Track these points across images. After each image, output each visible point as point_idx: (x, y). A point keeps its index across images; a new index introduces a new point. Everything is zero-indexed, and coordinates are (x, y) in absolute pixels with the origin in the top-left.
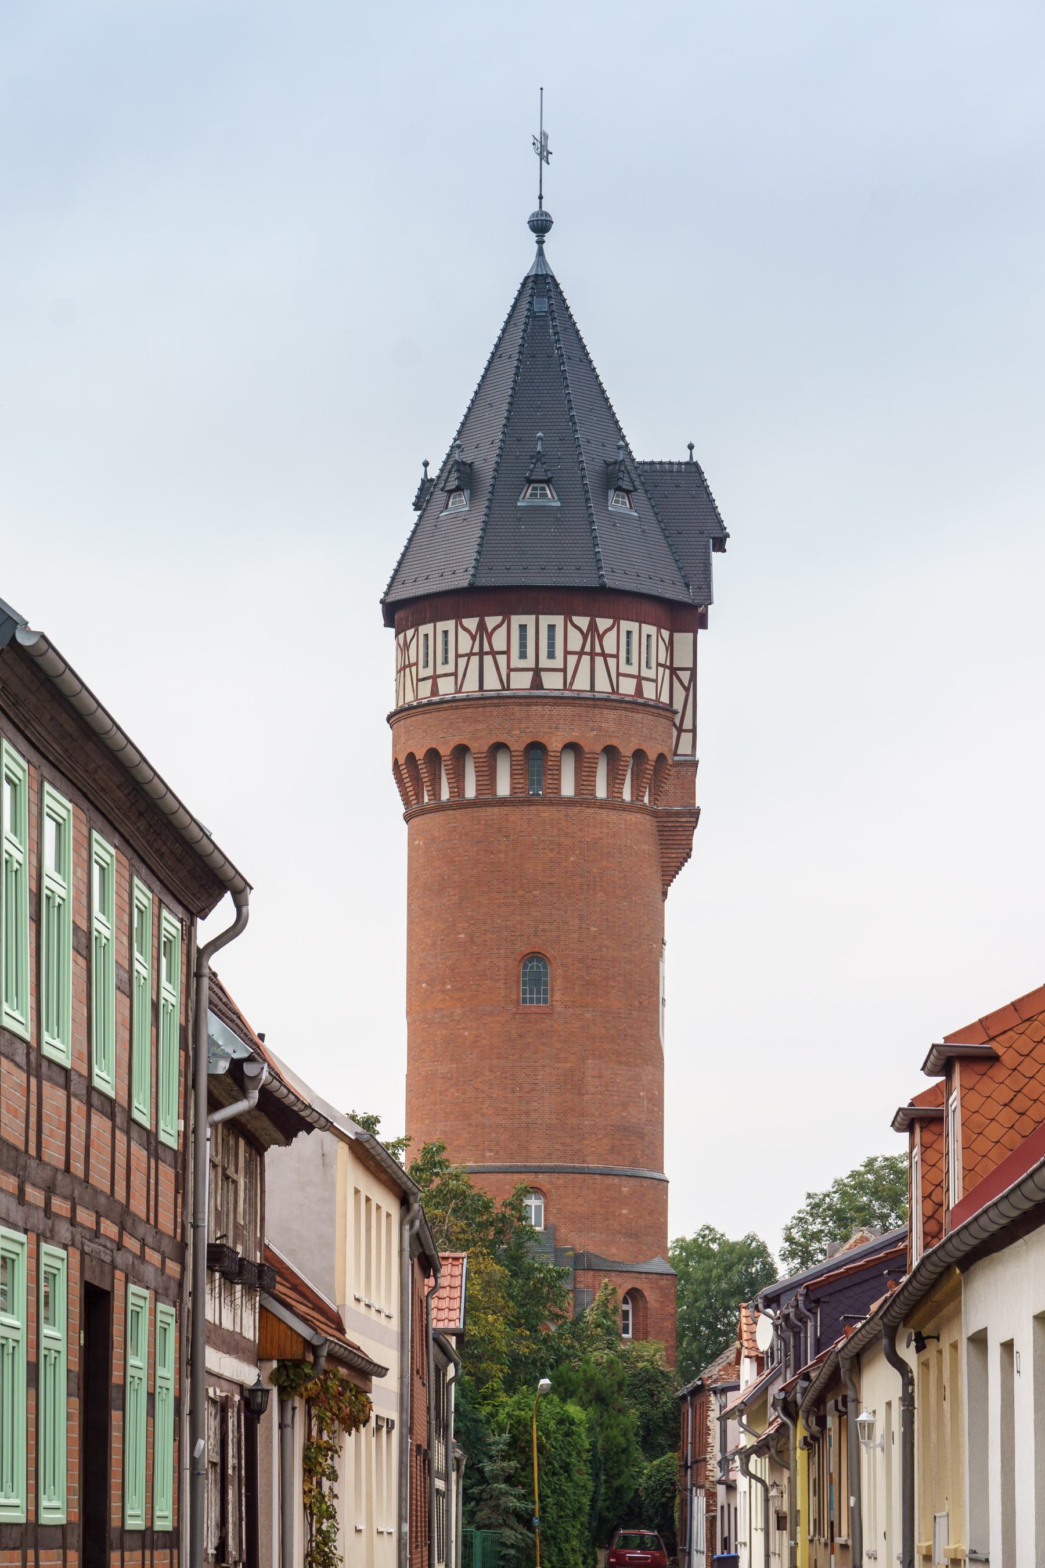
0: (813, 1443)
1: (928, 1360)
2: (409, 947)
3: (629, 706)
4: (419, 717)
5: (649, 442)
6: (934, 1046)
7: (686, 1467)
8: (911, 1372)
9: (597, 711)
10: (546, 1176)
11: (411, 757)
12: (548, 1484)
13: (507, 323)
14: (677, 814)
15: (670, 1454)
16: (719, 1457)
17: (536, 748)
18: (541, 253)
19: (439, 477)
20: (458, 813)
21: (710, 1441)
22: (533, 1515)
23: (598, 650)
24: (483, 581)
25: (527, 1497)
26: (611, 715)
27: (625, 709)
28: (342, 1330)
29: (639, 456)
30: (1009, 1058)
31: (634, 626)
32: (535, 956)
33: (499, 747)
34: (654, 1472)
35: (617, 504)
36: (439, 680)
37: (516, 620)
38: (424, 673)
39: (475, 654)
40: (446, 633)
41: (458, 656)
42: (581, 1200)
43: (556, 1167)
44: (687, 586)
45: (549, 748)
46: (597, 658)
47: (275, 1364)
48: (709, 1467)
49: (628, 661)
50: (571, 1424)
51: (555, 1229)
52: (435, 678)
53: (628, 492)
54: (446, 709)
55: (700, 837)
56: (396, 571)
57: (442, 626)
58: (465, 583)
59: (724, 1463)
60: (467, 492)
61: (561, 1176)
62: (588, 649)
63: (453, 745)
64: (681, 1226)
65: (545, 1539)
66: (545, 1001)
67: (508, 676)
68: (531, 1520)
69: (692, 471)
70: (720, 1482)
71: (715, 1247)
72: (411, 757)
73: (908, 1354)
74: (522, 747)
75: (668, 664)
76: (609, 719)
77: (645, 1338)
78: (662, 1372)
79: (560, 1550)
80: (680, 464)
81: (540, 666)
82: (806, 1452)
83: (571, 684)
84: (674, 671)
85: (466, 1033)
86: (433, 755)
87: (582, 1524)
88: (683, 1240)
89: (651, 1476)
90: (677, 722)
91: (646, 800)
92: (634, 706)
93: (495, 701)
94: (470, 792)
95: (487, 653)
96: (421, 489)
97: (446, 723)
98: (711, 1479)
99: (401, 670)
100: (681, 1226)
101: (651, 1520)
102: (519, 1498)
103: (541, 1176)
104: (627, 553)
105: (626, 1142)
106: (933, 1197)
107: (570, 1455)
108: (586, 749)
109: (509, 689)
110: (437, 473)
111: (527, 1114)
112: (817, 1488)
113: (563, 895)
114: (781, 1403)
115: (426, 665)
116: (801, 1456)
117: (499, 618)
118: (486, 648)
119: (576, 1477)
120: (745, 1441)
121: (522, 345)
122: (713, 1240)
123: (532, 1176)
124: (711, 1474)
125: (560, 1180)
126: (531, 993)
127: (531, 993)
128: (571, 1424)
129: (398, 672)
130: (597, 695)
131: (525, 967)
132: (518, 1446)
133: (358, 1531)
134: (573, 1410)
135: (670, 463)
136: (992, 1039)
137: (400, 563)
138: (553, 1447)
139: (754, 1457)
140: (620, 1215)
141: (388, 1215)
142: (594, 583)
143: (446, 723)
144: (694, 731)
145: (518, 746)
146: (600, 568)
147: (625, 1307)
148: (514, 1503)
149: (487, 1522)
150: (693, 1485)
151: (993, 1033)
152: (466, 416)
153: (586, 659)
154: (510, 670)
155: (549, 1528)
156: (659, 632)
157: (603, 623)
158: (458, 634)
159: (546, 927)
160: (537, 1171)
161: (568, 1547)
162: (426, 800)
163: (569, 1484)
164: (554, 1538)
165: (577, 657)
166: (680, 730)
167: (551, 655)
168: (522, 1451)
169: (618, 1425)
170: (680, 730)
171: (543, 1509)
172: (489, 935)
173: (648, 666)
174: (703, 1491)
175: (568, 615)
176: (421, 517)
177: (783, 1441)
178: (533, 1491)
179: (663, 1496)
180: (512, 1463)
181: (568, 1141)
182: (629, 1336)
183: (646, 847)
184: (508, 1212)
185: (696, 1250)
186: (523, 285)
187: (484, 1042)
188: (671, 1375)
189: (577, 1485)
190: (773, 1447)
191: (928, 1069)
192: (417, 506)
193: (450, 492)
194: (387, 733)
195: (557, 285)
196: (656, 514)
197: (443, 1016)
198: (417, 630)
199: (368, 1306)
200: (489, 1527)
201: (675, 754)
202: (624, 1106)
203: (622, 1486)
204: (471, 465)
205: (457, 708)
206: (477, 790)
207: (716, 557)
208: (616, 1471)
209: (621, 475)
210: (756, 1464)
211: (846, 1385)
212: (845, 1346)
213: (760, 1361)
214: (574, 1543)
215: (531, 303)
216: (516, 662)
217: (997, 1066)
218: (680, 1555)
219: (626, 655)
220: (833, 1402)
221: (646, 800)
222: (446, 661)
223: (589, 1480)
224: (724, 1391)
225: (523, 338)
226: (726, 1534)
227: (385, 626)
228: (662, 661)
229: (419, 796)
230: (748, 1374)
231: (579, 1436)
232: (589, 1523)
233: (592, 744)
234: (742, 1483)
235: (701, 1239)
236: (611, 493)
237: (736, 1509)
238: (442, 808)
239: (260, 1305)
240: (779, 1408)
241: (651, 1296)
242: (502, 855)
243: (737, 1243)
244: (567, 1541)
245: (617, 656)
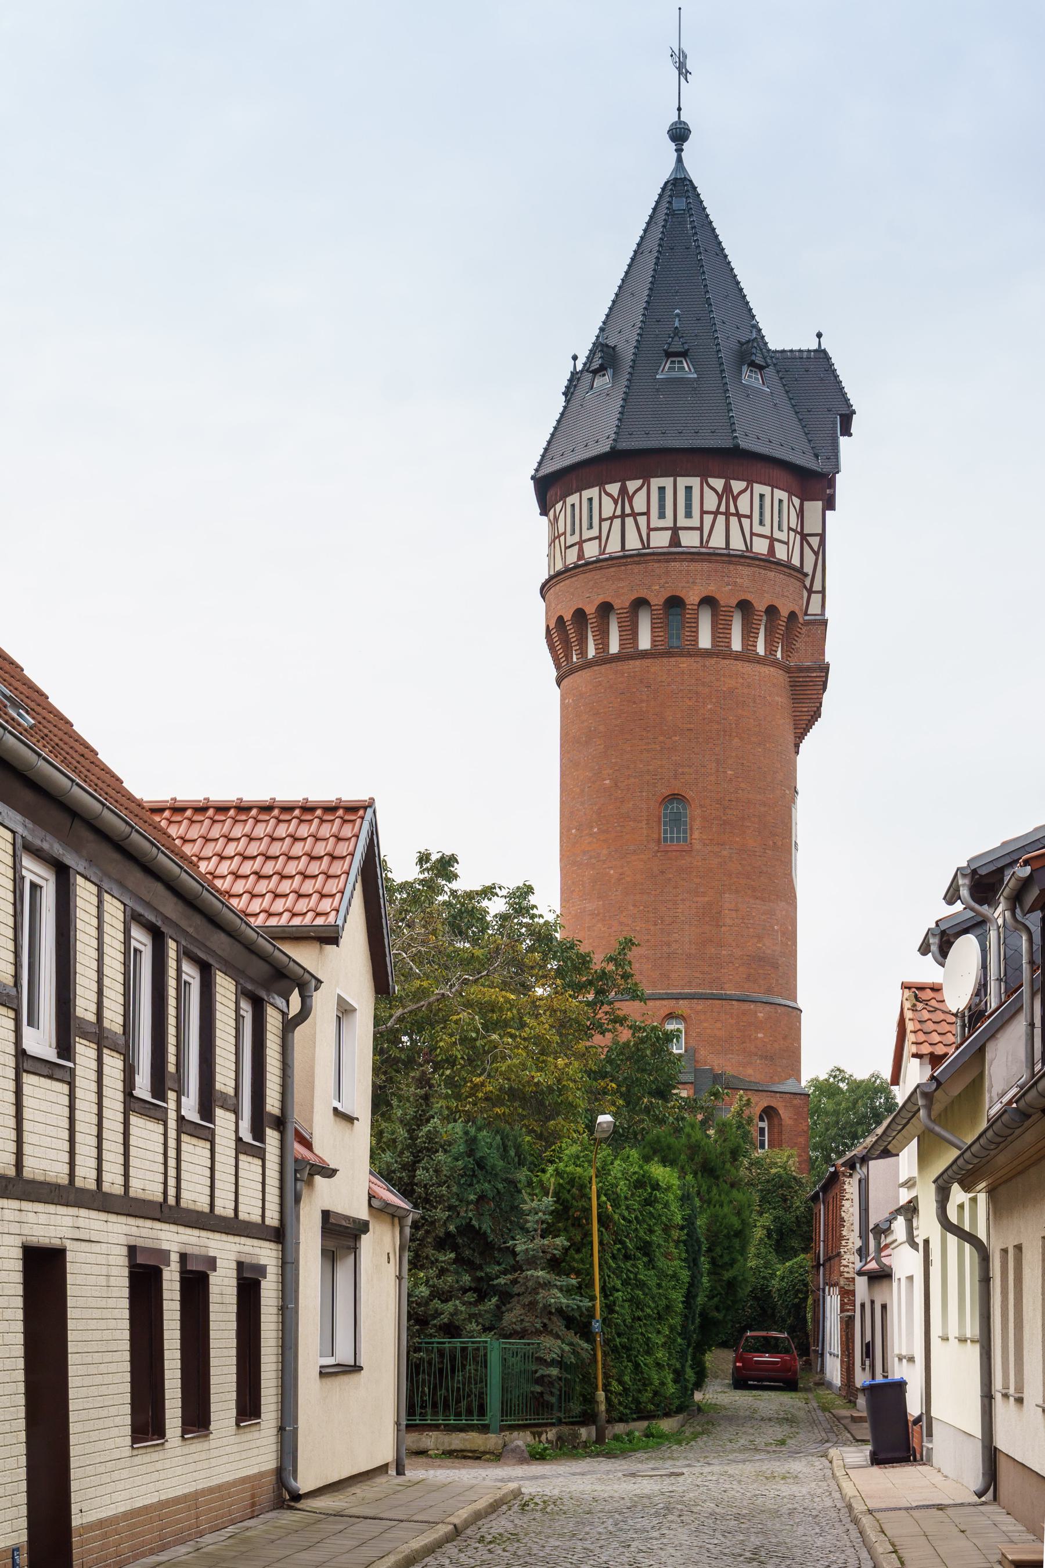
2: (561, 799)
3: (762, 564)
4: (567, 582)
5: (782, 333)
7: (818, 1265)
9: (732, 567)
10: (686, 1002)
11: (560, 619)
12: (617, 1272)
13: (648, 224)
14: (809, 669)
15: (802, 1256)
17: (675, 603)
18: (679, 160)
20: (603, 668)
21: (844, 1233)
22: (592, 1316)
23: (732, 510)
24: (623, 445)
25: (584, 1288)
26: (745, 571)
27: (758, 566)
31: (766, 490)
32: (675, 797)
33: (641, 603)
34: (787, 1274)
35: (750, 378)
37: (656, 483)
38: (571, 540)
39: (617, 517)
41: (601, 520)
42: (719, 1025)
43: (695, 993)
44: (816, 456)
46: (731, 518)
49: (761, 523)
50: (653, 1189)
51: (695, 1051)
52: (581, 543)
53: (761, 368)
54: (591, 571)
55: (829, 700)
56: (546, 450)
57: (587, 494)
60: (610, 371)
61: (700, 1001)
62: (723, 509)
63: (597, 603)
64: (813, 1068)
65: (613, 1350)
66: (685, 839)
67: (648, 535)
68: (590, 1323)
69: (821, 356)
71: (843, 1086)
72: (560, 619)
74: (661, 601)
75: (799, 529)
76: (744, 574)
77: (780, 1146)
78: (795, 1178)
79: (637, 1366)
80: (809, 351)
83: (708, 542)
84: (804, 537)
85: (612, 872)
87: (672, 1329)
88: (816, 1080)
89: (783, 1278)
90: (808, 584)
91: (779, 655)
92: (767, 564)
93: (636, 559)
95: (628, 515)
96: (570, 381)
97: (591, 583)
98: (846, 1275)
99: (552, 543)
100: (813, 1068)
101: (784, 1321)
102: (568, 1291)
103: (681, 1002)
104: (762, 422)
105: (761, 971)
107: (651, 1231)
109: (649, 548)
111: (668, 944)
113: (701, 740)
115: (573, 533)
117: (639, 482)
118: (628, 511)
119: (661, 1263)
121: (661, 239)
122: (843, 1080)
124: (846, 1269)
125: (700, 1006)
126: (672, 832)
127: (672, 832)
128: (653, 1189)
130: (732, 552)
131: (666, 809)
132: (568, 1213)
134: (659, 1171)
135: (800, 351)
137: (549, 443)
138: (624, 1219)
140: (756, 1038)
142: (728, 444)
143: (591, 583)
144: (823, 592)
145: (657, 600)
147: (761, 1124)
148: (557, 1298)
149: (518, 1328)
150: (825, 1284)
152: (610, 309)
153: (721, 519)
154: (650, 529)
155: (619, 1335)
156: (790, 499)
157: (737, 486)
158: (600, 499)
159: (686, 770)
160: (677, 997)
161: (650, 1360)
162: (575, 660)
163: (652, 1272)
164: (627, 1349)
165: (712, 516)
166: (810, 591)
167: (689, 515)
168: (577, 1223)
169: (731, 1202)
170: (810, 591)
171: (609, 1308)
172: (633, 780)
173: (780, 529)
174: (837, 1290)
175: (704, 477)
178: (592, 1280)
179: (796, 1296)
180: (558, 1241)
181: (707, 969)
183: (778, 699)
184: (611, 967)
185: (826, 1089)
186: (663, 189)
187: (628, 879)
188: (804, 1181)
189: (662, 1274)
192: (565, 394)
195: (695, 188)
196: (787, 392)
197: (591, 858)
198: (565, 502)
200: (522, 1334)
201: (806, 614)
202: (760, 938)
203: (735, 1278)
204: (614, 348)
205: (601, 568)
206: (620, 645)
207: (843, 441)
208: (726, 1259)
209: (754, 351)
214: (659, 1355)
215: (670, 202)
216: (655, 522)
218: (812, 1356)
219: (761, 517)
221: (779, 655)
222: (591, 527)
223: (681, 1268)
225: (662, 232)
227: (541, 514)
228: (793, 525)
229: (568, 657)
231: (666, 1205)
232: (683, 1326)
233: (727, 598)
235: (831, 1080)
236: (745, 368)
237: (884, 1307)
238: (588, 665)
241: (785, 1115)
242: (644, 705)
243: (863, 1081)
244: (649, 1352)
245: (750, 517)
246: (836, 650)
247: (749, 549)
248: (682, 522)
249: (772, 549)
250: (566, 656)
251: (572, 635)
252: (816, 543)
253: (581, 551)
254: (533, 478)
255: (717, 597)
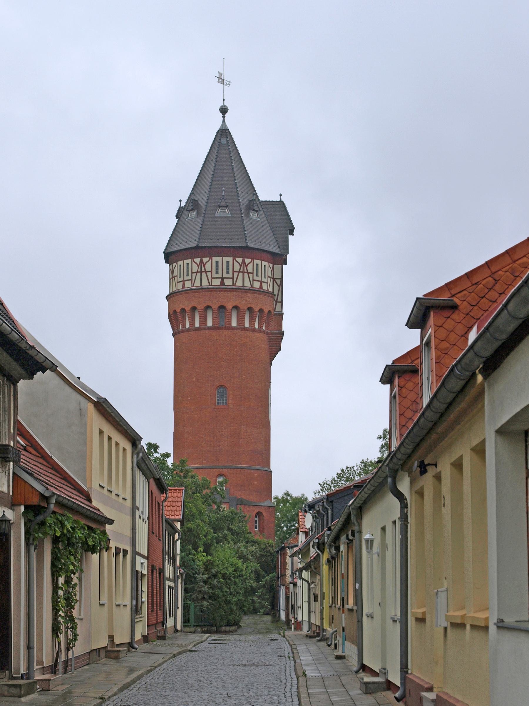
0: (332, 561)
1: (422, 488)
5: (265, 193)
6: (418, 299)
8: (406, 499)
9: (245, 294)
10: (226, 470)
16: (290, 574)
18: (224, 121)
19: (185, 206)
23: (245, 271)
28: (90, 501)
29: (261, 199)
30: (464, 306)
31: (259, 262)
33: (208, 307)
35: (253, 215)
36: (185, 282)
37: (215, 259)
38: (180, 279)
40: (188, 264)
41: (192, 273)
45: (227, 308)
47: (22, 508)
48: (287, 578)
49: (257, 275)
52: (184, 281)
53: (257, 211)
57: (186, 261)
58: (195, 245)
59: (293, 574)
62: (242, 270)
64: (278, 491)
69: (281, 204)
70: (291, 583)
73: (404, 486)
81: (224, 276)
82: (328, 566)
84: (274, 279)
86: (183, 310)
91: (264, 328)
94: (197, 325)
95: (204, 272)
99: (171, 278)
106: (405, 414)
108: (241, 308)
109: (212, 285)
110: (185, 204)
111: (219, 446)
112: (334, 581)
114: (316, 544)
115: (180, 277)
116: (325, 568)
117: (208, 259)
118: (203, 270)
120: (300, 566)
123: (221, 470)
126: (220, 401)
129: (170, 279)
130: (245, 288)
133: (102, 605)
136: (453, 296)
139: (304, 571)
141: (124, 450)
142: (245, 245)
144: (282, 302)
145: (215, 307)
146: (246, 240)
147: (256, 519)
150: (281, 585)
151: (453, 292)
153: (241, 274)
154: (212, 278)
156: (268, 264)
157: (247, 261)
158: (191, 264)
160: (222, 468)
162: (181, 328)
167: (228, 272)
170: (277, 302)
173: (265, 277)
176: (178, 221)
177: (317, 563)
182: (258, 529)
186: (217, 133)
190: (313, 567)
191: (411, 324)
192: (177, 217)
193: (189, 211)
194: (166, 303)
195: (230, 133)
198: (177, 263)
199: (110, 491)
207: (290, 237)
210: (305, 574)
211: (354, 524)
212: (353, 503)
213: (306, 533)
217: (457, 312)
220: (345, 536)
221: (264, 328)
222: (188, 275)
224: (292, 547)
226: (293, 603)
228: (270, 275)
230: (302, 538)
233: (243, 306)
234: (299, 582)
236: (251, 211)
239: (14, 473)
240: (316, 547)
245: (253, 273)
246: (286, 325)
247: (252, 286)
248: (225, 275)
249: (261, 285)
250: (177, 326)
251: (180, 317)
252: (279, 282)
253: (184, 284)
254: (164, 253)
255: (239, 306)
